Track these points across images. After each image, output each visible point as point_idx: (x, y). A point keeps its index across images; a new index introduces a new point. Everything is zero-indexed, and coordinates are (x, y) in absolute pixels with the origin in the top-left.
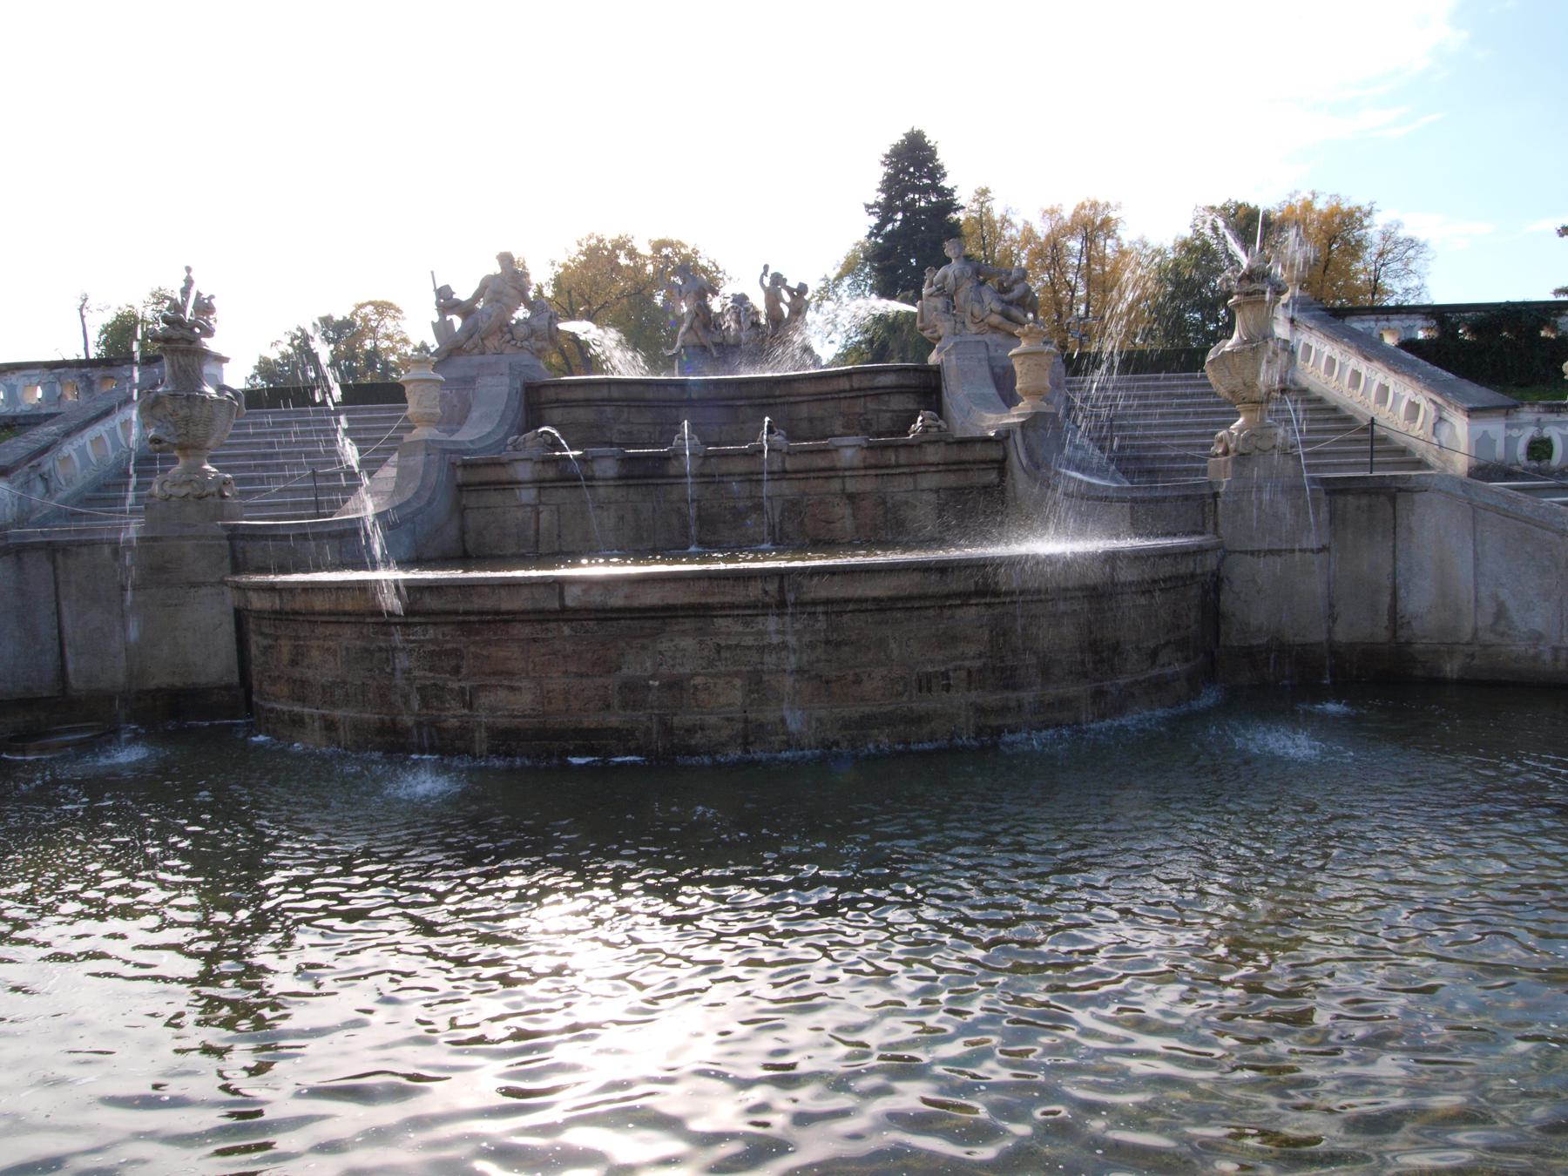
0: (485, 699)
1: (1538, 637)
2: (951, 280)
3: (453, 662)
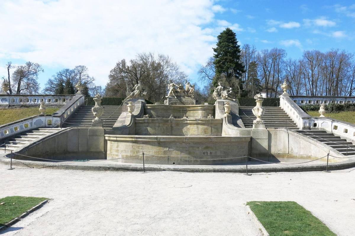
2: (219, 89)
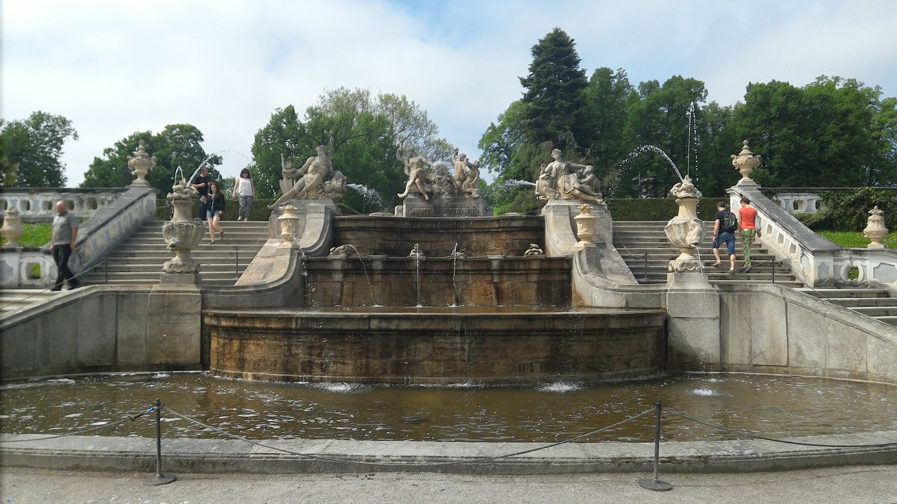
1: (816, 364)
2: (554, 170)
3: (318, 351)
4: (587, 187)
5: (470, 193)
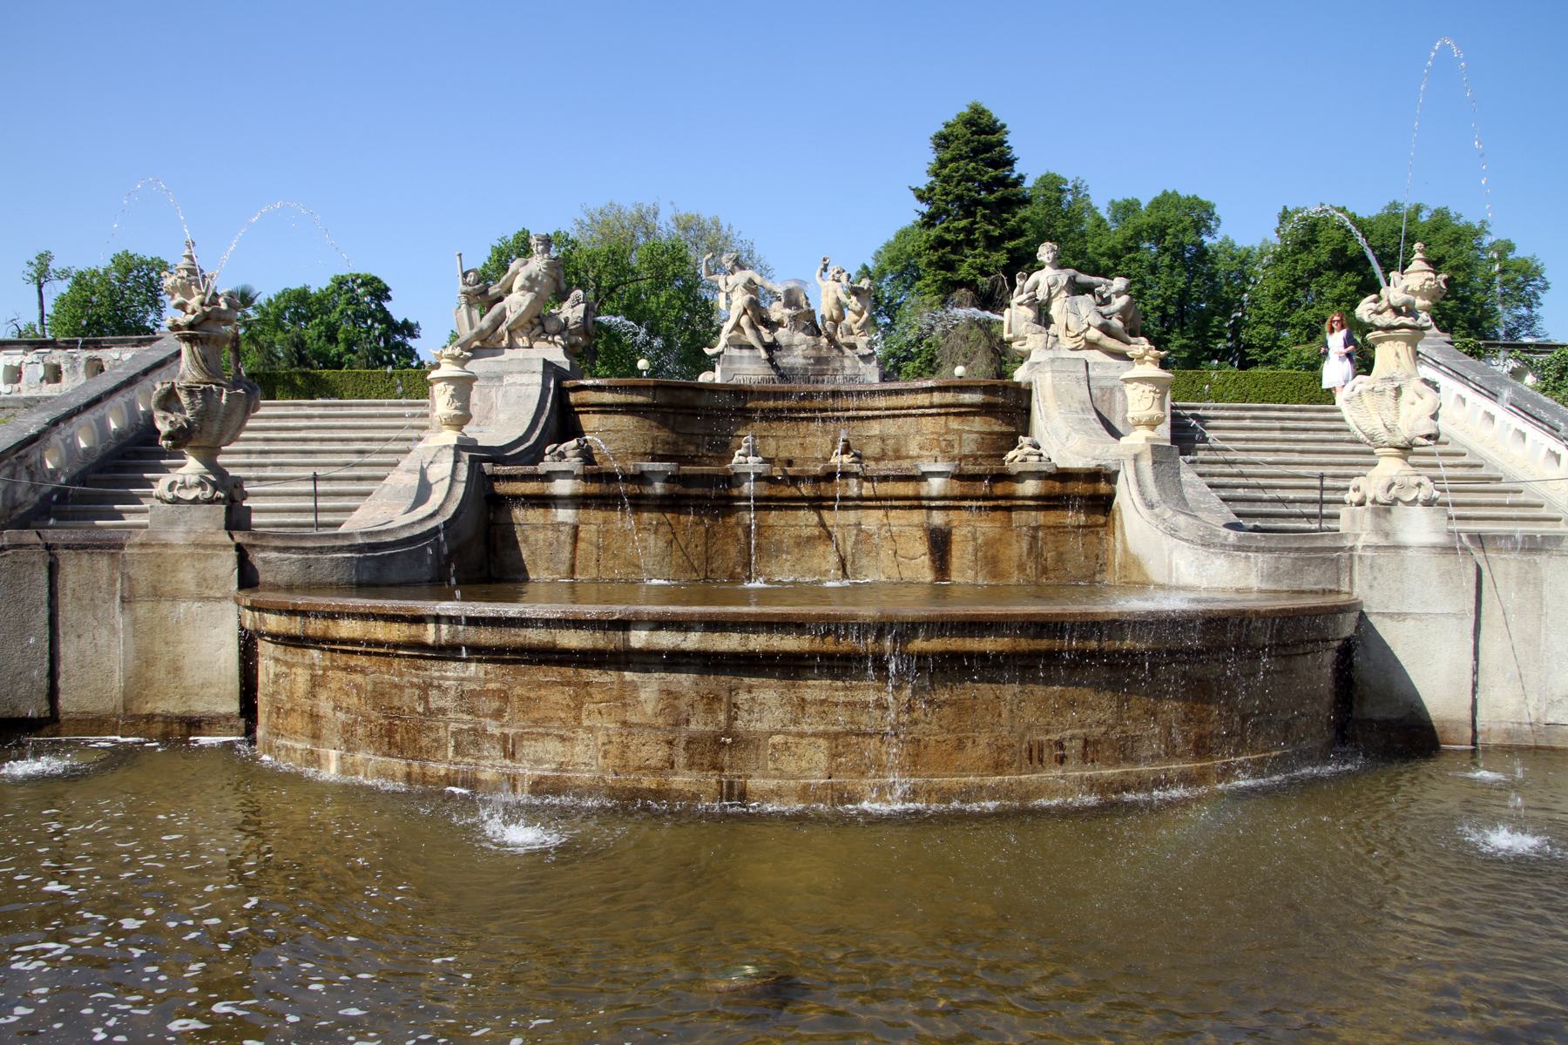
0: (529, 749)
3: (496, 704)
4: (1116, 323)
5: (852, 346)
